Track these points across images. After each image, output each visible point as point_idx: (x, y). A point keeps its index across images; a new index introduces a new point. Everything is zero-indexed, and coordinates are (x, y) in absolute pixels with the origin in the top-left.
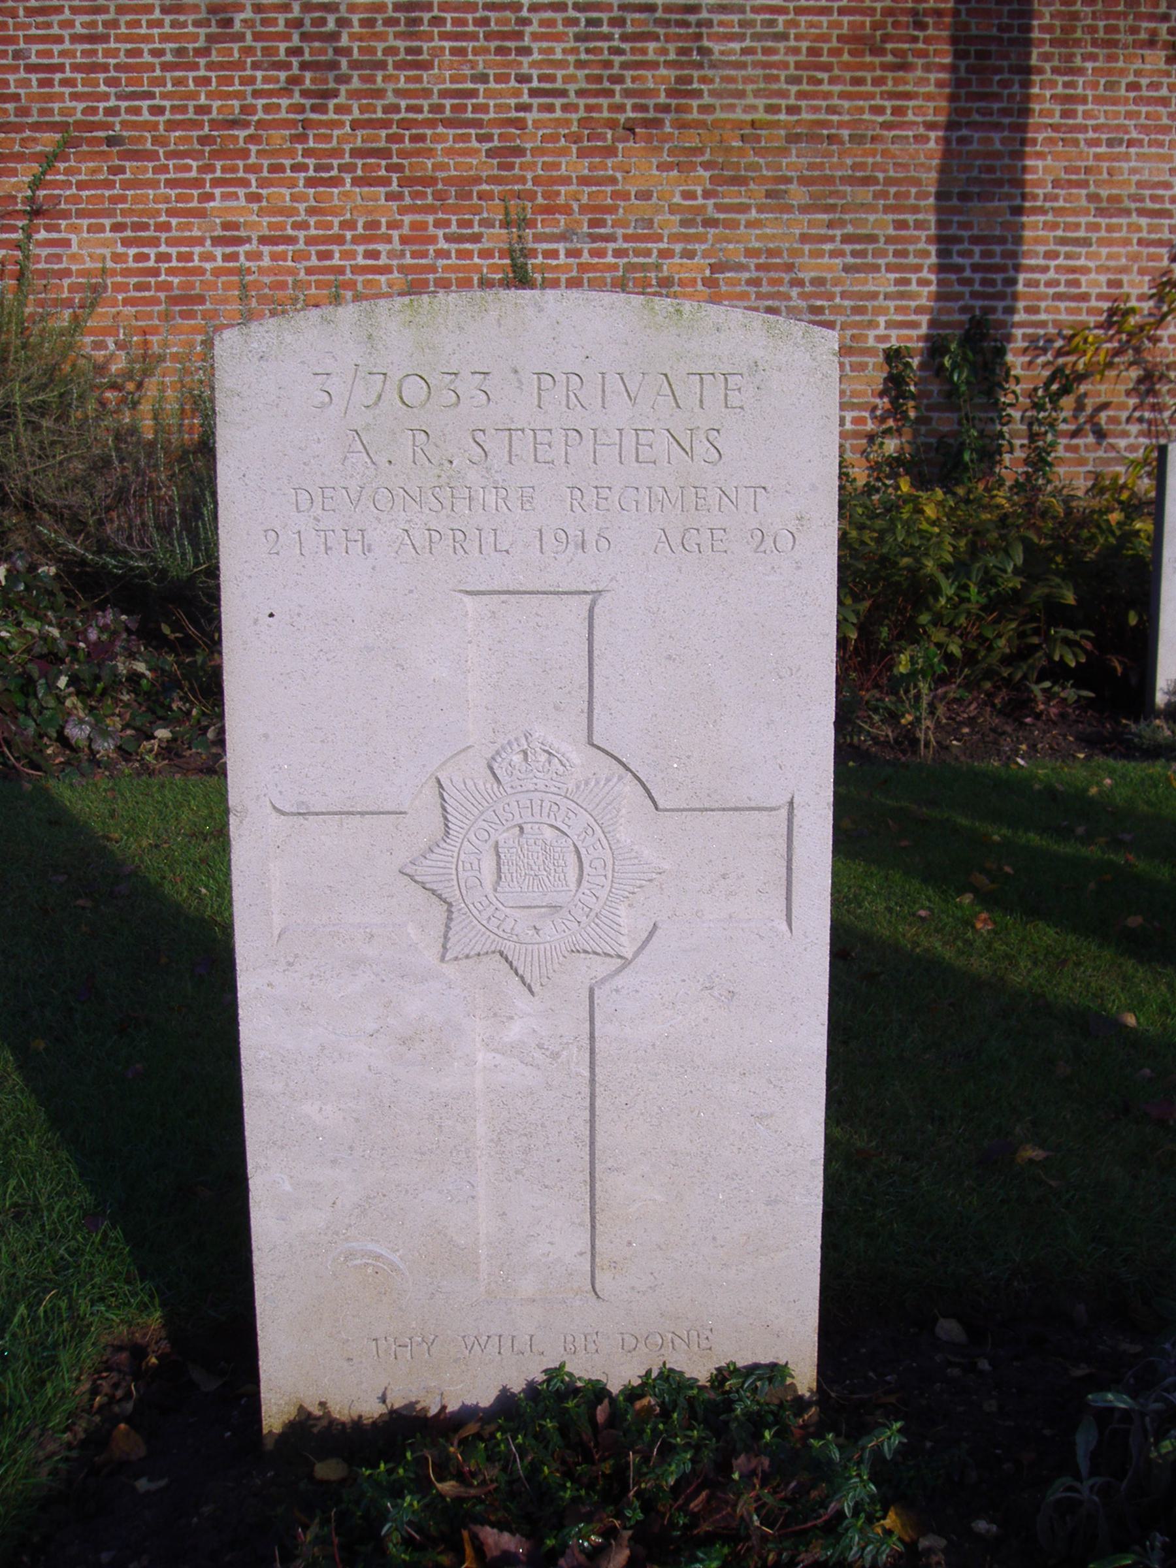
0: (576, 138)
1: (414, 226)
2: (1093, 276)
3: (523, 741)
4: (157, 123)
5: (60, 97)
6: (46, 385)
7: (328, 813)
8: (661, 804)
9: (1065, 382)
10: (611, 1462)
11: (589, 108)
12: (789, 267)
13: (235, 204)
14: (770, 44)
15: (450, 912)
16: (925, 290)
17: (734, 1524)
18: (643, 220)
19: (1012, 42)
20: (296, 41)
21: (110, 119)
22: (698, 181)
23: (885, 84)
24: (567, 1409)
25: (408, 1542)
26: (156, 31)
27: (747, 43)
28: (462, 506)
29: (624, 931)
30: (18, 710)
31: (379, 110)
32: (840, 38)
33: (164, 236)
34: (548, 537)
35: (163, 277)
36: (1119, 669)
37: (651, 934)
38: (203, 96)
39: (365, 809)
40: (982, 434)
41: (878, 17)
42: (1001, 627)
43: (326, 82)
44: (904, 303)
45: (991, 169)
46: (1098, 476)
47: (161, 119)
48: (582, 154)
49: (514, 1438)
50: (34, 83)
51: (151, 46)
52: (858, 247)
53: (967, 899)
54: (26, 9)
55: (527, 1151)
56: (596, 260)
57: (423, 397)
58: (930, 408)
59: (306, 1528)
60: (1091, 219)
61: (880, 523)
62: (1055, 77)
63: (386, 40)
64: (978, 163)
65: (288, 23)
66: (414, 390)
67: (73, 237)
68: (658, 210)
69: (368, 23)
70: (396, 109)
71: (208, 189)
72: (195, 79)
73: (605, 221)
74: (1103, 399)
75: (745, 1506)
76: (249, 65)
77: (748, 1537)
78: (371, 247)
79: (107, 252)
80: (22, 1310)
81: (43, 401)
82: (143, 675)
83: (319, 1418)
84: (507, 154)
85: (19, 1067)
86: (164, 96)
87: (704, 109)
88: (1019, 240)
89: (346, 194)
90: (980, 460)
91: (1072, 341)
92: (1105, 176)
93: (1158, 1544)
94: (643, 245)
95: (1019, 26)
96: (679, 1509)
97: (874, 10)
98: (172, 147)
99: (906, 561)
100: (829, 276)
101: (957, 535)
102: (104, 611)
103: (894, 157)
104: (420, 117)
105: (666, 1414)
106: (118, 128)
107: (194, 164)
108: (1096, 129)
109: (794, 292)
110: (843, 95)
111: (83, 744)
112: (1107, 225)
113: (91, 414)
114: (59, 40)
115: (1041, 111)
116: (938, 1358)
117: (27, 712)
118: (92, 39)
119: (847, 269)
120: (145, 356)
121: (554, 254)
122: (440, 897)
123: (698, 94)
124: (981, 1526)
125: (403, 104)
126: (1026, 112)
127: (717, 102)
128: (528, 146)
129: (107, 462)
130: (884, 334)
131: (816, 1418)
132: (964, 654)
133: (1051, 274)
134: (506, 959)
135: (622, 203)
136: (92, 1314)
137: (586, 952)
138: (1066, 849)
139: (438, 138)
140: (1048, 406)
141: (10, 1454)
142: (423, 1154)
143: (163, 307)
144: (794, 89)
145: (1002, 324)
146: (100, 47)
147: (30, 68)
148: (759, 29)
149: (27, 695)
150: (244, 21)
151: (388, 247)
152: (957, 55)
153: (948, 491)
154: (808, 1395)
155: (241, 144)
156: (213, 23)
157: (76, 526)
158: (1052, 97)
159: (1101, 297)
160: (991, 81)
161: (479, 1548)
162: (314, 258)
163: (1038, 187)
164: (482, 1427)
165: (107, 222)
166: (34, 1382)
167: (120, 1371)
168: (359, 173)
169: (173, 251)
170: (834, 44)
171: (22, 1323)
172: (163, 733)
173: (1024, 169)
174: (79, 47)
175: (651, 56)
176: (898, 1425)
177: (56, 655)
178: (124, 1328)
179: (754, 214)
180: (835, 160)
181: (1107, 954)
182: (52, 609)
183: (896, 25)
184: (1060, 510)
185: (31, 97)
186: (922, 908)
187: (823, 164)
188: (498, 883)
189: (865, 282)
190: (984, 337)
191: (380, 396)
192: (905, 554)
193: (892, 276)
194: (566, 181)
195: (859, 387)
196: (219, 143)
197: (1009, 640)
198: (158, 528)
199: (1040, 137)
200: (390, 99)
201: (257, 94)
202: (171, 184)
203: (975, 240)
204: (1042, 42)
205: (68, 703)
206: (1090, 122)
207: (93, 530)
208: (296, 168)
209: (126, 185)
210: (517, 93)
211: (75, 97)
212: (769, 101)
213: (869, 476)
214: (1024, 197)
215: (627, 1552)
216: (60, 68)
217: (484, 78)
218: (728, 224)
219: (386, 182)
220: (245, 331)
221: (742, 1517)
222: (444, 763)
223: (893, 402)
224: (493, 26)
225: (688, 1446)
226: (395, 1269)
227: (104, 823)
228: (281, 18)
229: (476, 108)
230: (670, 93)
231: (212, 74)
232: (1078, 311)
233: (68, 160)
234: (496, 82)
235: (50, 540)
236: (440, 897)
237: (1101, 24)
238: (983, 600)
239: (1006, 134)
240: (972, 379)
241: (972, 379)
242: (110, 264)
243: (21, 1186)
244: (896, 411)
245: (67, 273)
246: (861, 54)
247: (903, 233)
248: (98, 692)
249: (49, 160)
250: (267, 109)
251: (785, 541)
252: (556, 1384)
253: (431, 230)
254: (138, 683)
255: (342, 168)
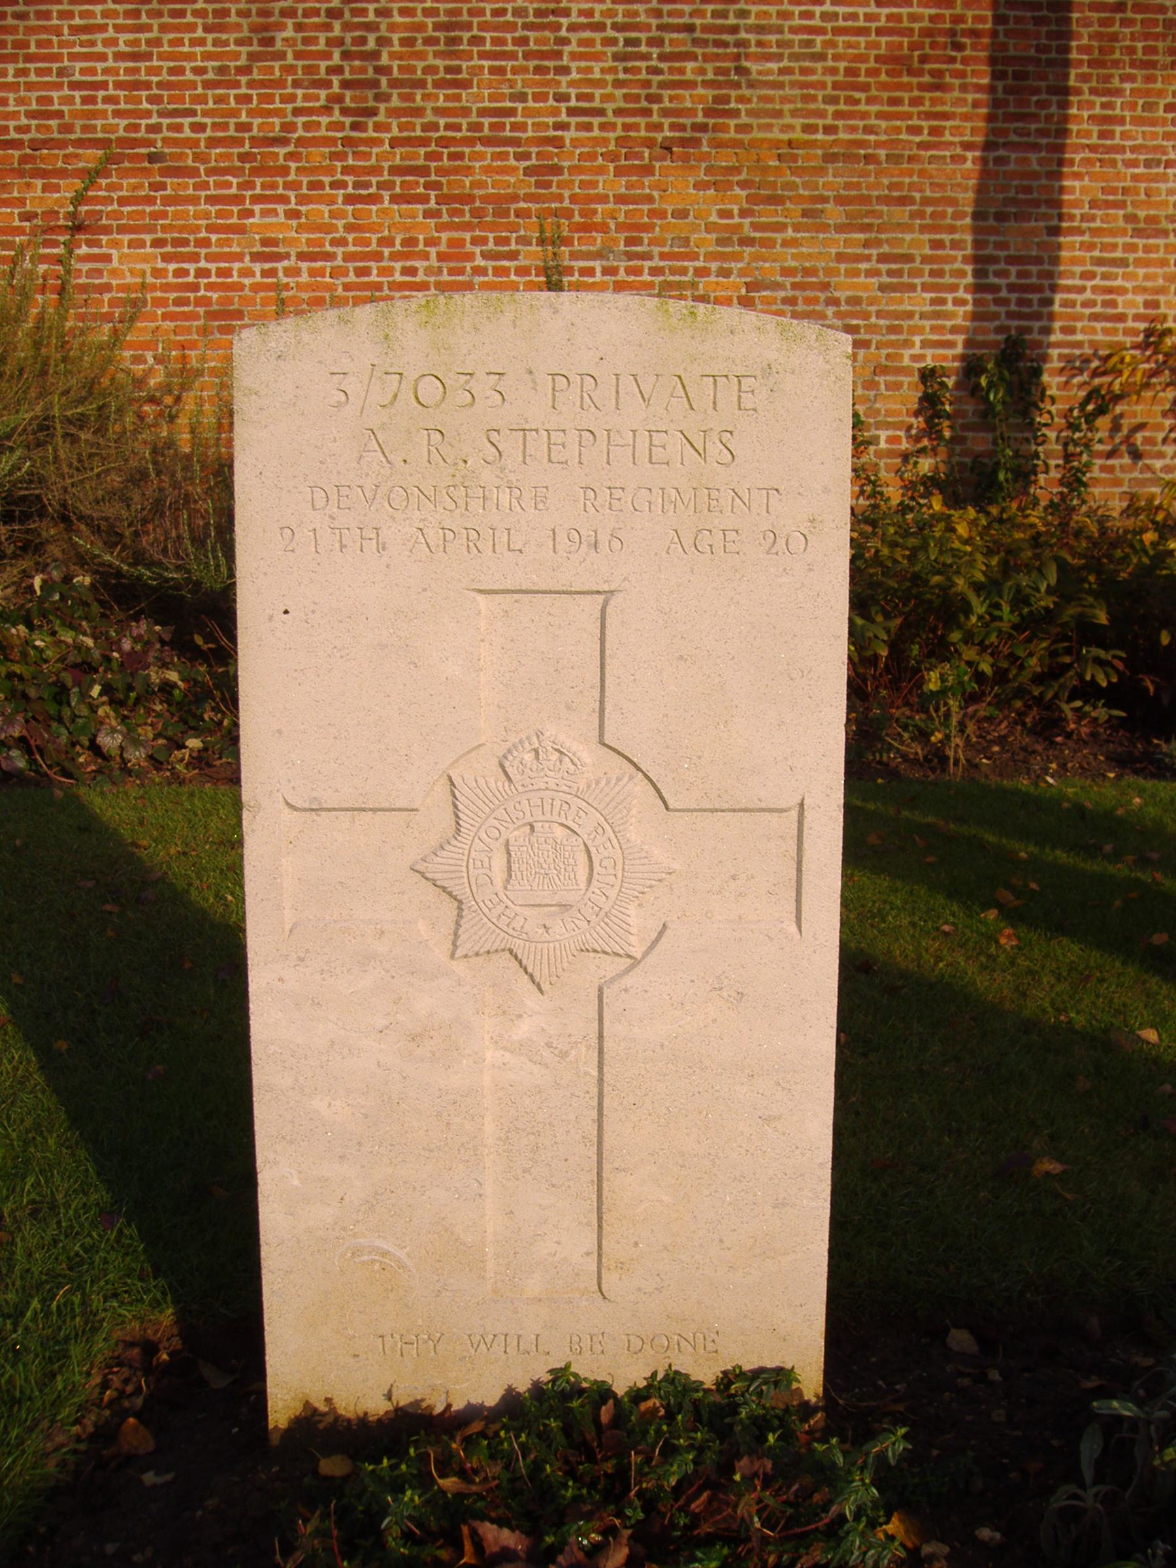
0: (612, 157)
1: (452, 243)
2: (1130, 296)
3: (535, 739)
4: (199, 140)
5: (103, 114)
6: (85, 398)
7: (342, 810)
8: (672, 803)
9: (1100, 402)
10: (614, 1462)
11: (627, 127)
12: (825, 286)
13: (274, 220)
14: (807, 64)
15: (460, 909)
16: (961, 310)
17: (735, 1526)
18: (679, 238)
19: (1050, 63)
20: (336, 59)
21: (152, 136)
22: (735, 199)
23: (922, 104)
24: (571, 1409)
25: (407, 1536)
26: (198, 49)
27: (785, 63)
28: (476, 505)
29: (634, 930)
30: (52, 718)
31: (418, 128)
32: (878, 59)
33: (203, 251)
34: (561, 537)
35: (202, 293)
36: (1151, 689)
37: (661, 934)
38: (244, 114)
39: (377, 806)
40: (1017, 454)
41: (916, 38)
42: (1032, 646)
43: (366, 100)
44: (940, 322)
45: (1028, 190)
46: (1133, 497)
47: (202, 136)
48: (619, 172)
49: (517, 1437)
50: (78, 100)
51: (193, 64)
52: (894, 266)
53: (992, 914)
54: (71, 27)
55: (536, 1149)
56: (632, 278)
57: (439, 398)
58: (964, 427)
59: (306, 1521)
60: (1128, 240)
61: (912, 542)
62: (1093, 98)
63: (425, 59)
64: (1015, 183)
65: (330, 42)
66: (430, 390)
67: (114, 252)
68: (694, 228)
69: (408, 42)
70: (434, 127)
71: (247, 206)
72: (237, 97)
73: (641, 239)
74: (1139, 420)
75: (746, 1506)
76: (289, 83)
77: (749, 1539)
78: (409, 264)
79: (147, 267)
80: (35, 1304)
81: (82, 414)
82: (174, 686)
83: (324, 1414)
84: (544, 172)
85: (42, 1068)
86: (205, 113)
87: (740, 128)
88: (1055, 261)
89: (384, 212)
90: (1015, 480)
91: (1108, 363)
92: (1143, 197)
93: (1160, 1552)
94: (679, 264)
95: (1058, 47)
96: (680, 1509)
97: (912, 30)
98: (213, 164)
99: (936, 579)
100: (864, 295)
101: (989, 553)
102: (137, 621)
103: (931, 177)
104: (459, 135)
105: (670, 1416)
106: (159, 144)
107: (235, 181)
108: (1133, 149)
109: (830, 311)
110: (880, 115)
111: (115, 752)
112: (1145, 246)
113: (130, 427)
114: (102, 57)
115: (1078, 132)
116: (949, 1368)
117: (60, 720)
118: (135, 57)
119: (882, 288)
120: (182, 371)
121: (590, 272)
122: (450, 894)
123: (735, 113)
124: (985, 1533)
125: (442, 122)
126: (1064, 133)
127: (754, 122)
128: (566, 164)
129: (144, 475)
130: (919, 353)
131: (822, 1424)
132: (995, 673)
133: (1088, 295)
134: (516, 957)
135: (659, 222)
136: (105, 1310)
137: (595, 951)
138: (1093, 866)
139: (480, 156)
140: (1084, 426)
141: (18, 1446)
142: (431, 1151)
143: (201, 322)
144: (831, 109)
145: (1039, 345)
146: (142, 65)
147: (74, 86)
148: (796, 49)
149: (60, 703)
150: (285, 40)
151: (426, 264)
152: (995, 76)
153: (981, 510)
154: (814, 1400)
155: (281, 161)
156: (255, 42)
157: (112, 537)
158: (1090, 117)
159: (1137, 318)
160: (1029, 102)
161: (479, 1544)
162: (352, 274)
163: (1076, 207)
164: (486, 1425)
165: (148, 238)
166: (45, 1375)
167: (131, 1367)
168: (398, 190)
169: (213, 267)
170: (872, 64)
171: (34, 1318)
172: (194, 743)
173: (1062, 190)
174: (123, 65)
175: (689, 76)
176: (903, 1431)
177: (89, 664)
178: (136, 1325)
179: (790, 232)
180: (872, 179)
181: (1131, 971)
182: (86, 618)
183: (933, 45)
184: (1094, 529)
185: (75, 114)
186: (946, 923)
187: (859, 183)
188: (508, 881)
189: (901, 301)
190: (1020, 357)
191: (395, 396)
192: (939, 573)
193: (928, 296)
194: (603, 199)
195: (894, 407)
196: (259, 161)
197: (1040, 660)
198: (193, 540)
199: (1078, 157)
200: (430, 117)
201: (297, 112)
202: (211, 200)
203: (1011, 260)
204: (1080, 63)
205: (101, 712)
206: (1128, 143)
207: (129, 542)
208: (335, 185)
209: (167, 201)
210: (555, 112)
211: (117, 114)
212: (807, 121)
213: (903, 495)
214: (1061, 217)
215: (626, 1551)
216: (104, 85)
217: (522, 97)
218: (764, 243)
219: (424, 199)
220: (263, 330)
221: (743, 1519)
222: (456, 761)
223: (929, 421)
224: (532, 46)
225: (691, 1447)
226: (402, 1266)
227: (133, 830)
228: (322, 37)
229: (515, 127)
230: (708, 113)
231: (254, 92)
232: (1115, 331)
233: (110, 176)
234: (534, 101)
235: (87, 552)
236: (450, 894)
237: (1140, 45)
238: (1015, 619)
239: (1043, 154)
240: (1008, 399)
241: (1008, 399)
242: (150, 280)
243: (39, 1184)
244: (931, 430)
245: (107, 288)
246: (900, 74)
247: (939, 252)
248: (131, 702)
249: (91, 176)
250: (307, 126)
251: (798, 543)
252: (562, 1384)
253: (469, 247)
254: (171, 694)
255: (380, 186)
